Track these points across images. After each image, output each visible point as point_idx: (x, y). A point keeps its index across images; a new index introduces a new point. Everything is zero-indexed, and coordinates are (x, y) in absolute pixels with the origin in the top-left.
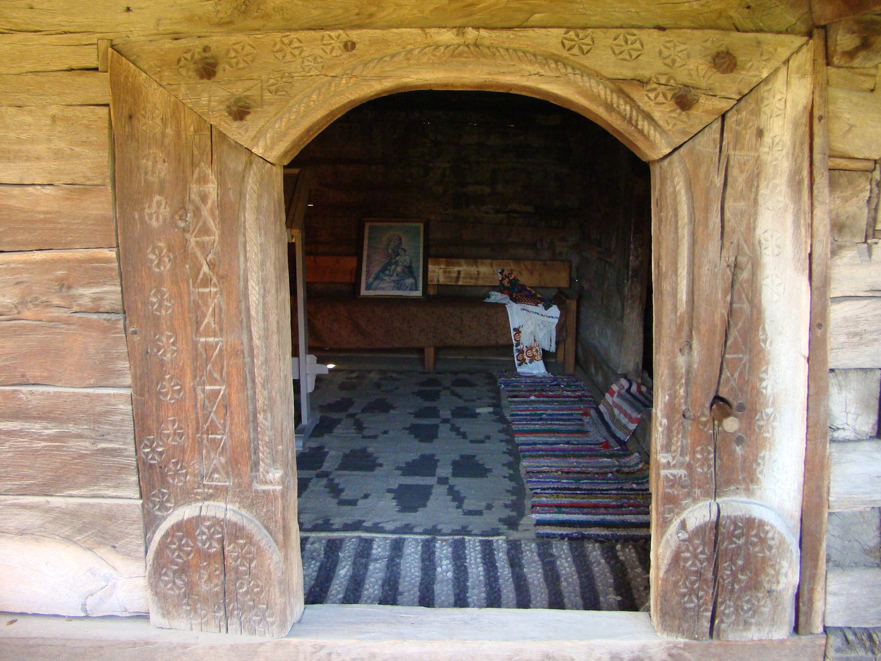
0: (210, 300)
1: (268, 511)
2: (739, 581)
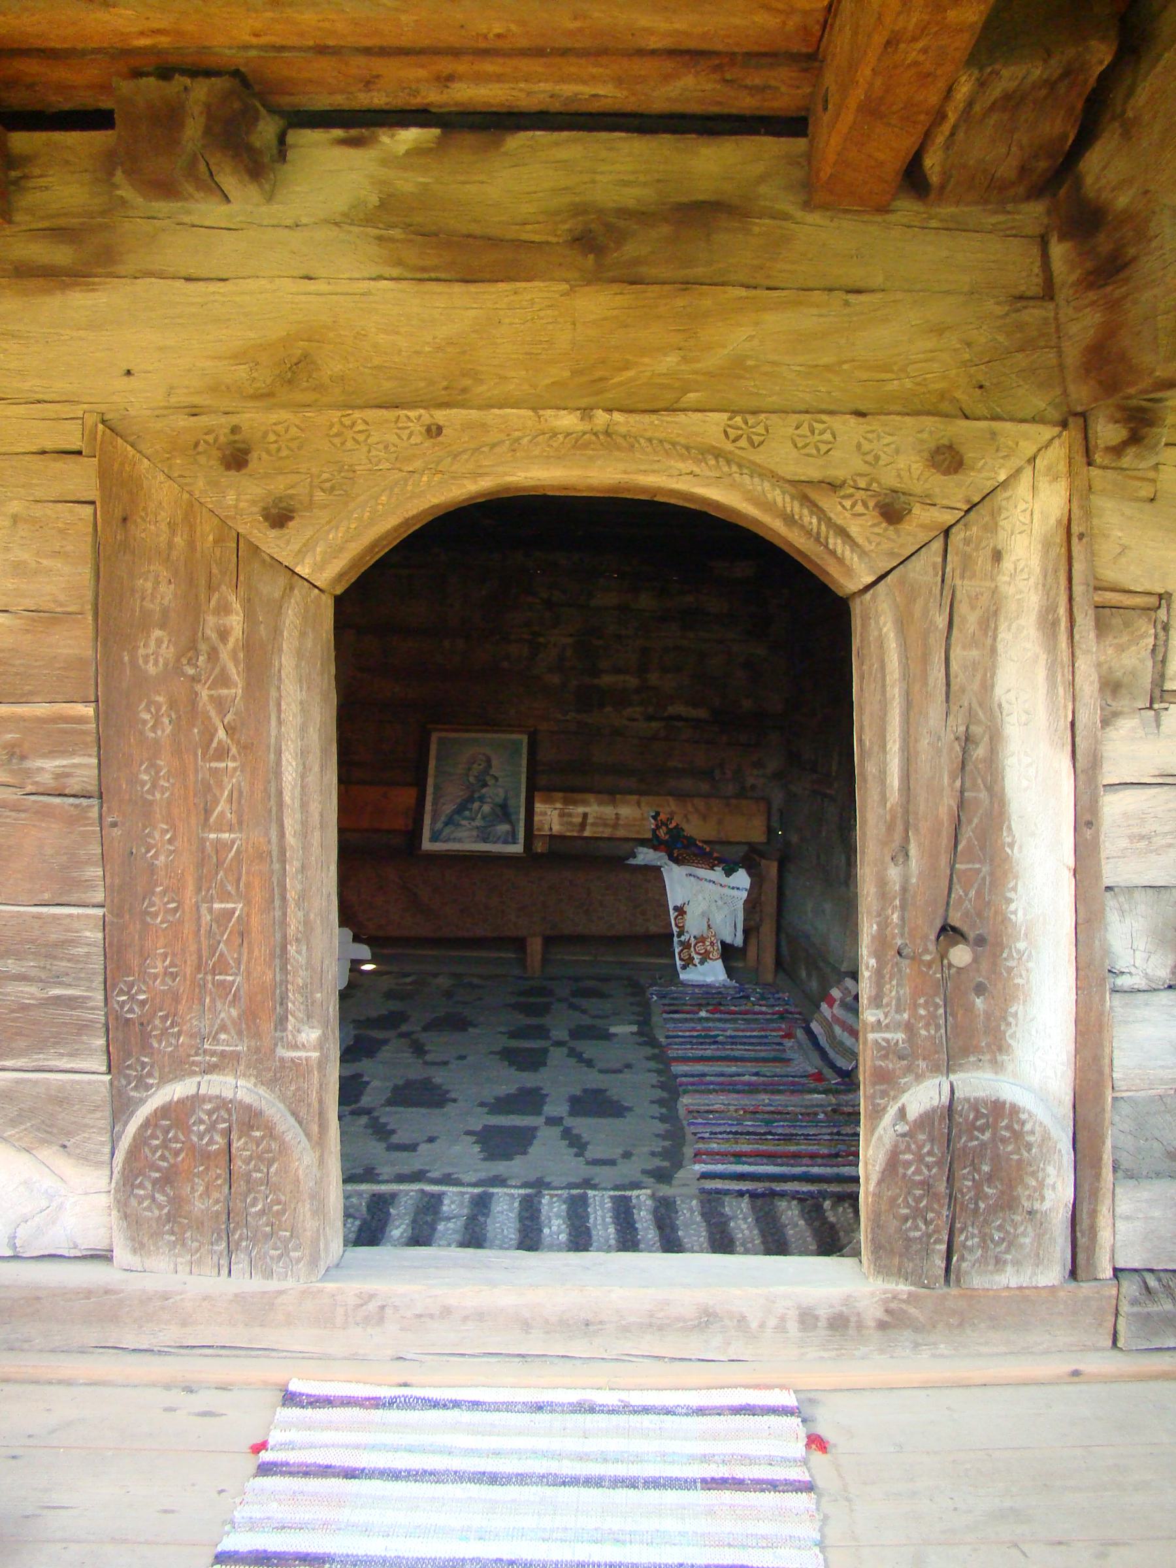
0: (226, 780)
1: (298, 1089)
2: (986, 1197)
